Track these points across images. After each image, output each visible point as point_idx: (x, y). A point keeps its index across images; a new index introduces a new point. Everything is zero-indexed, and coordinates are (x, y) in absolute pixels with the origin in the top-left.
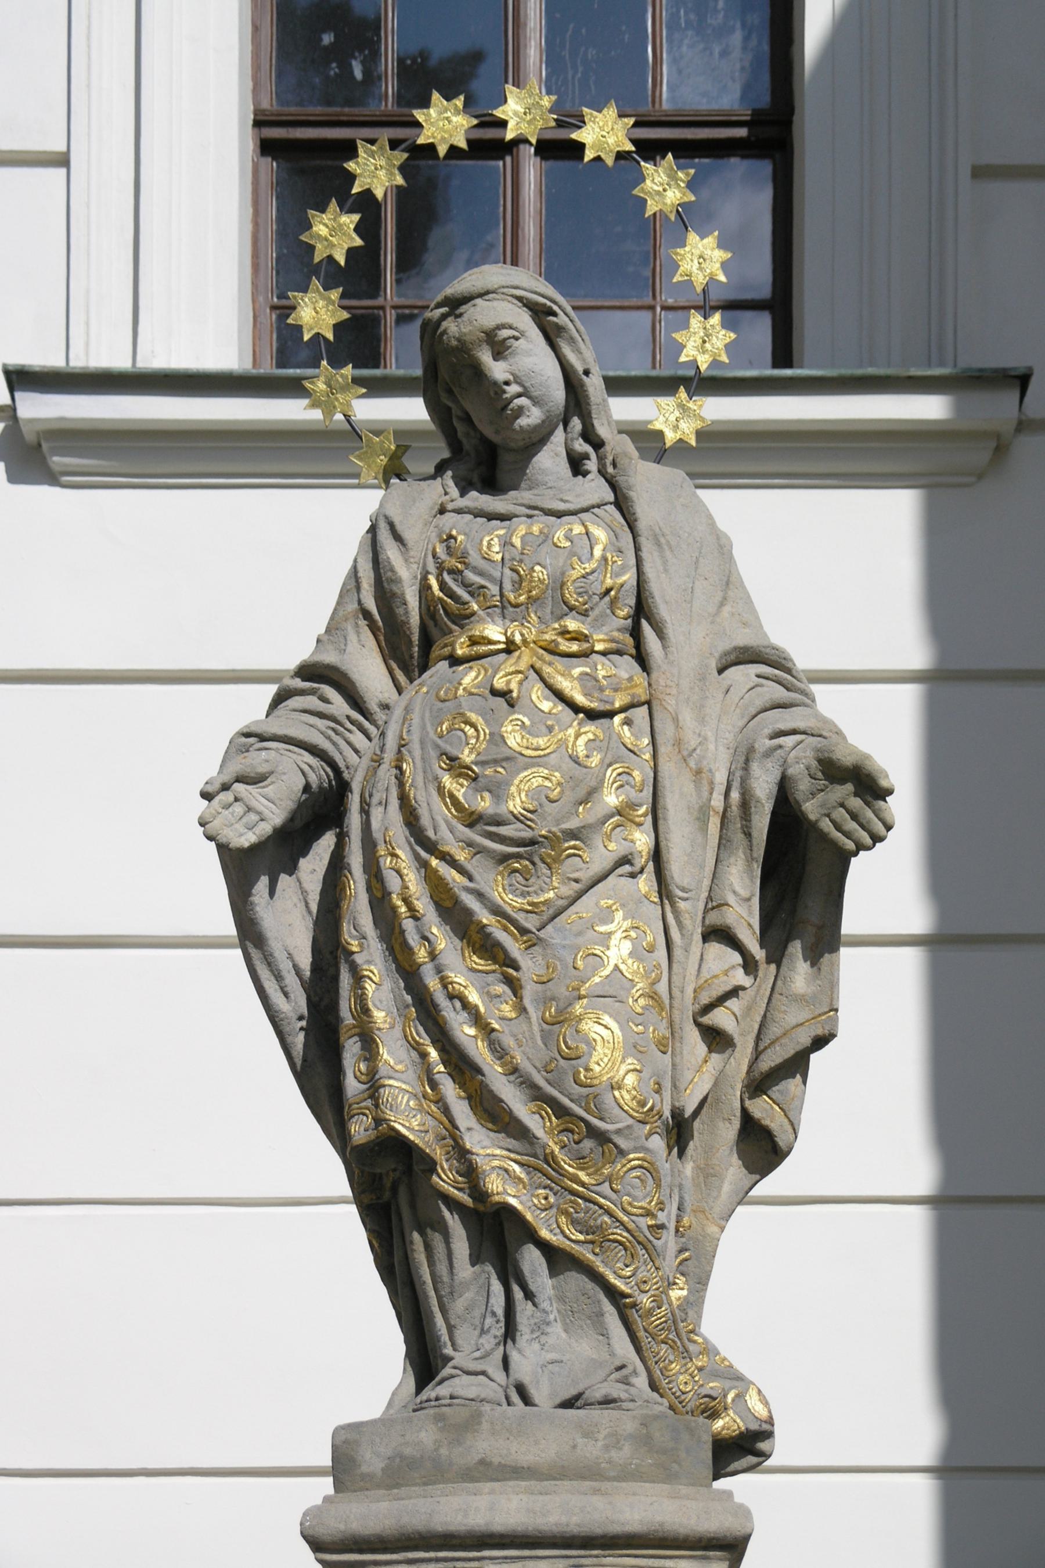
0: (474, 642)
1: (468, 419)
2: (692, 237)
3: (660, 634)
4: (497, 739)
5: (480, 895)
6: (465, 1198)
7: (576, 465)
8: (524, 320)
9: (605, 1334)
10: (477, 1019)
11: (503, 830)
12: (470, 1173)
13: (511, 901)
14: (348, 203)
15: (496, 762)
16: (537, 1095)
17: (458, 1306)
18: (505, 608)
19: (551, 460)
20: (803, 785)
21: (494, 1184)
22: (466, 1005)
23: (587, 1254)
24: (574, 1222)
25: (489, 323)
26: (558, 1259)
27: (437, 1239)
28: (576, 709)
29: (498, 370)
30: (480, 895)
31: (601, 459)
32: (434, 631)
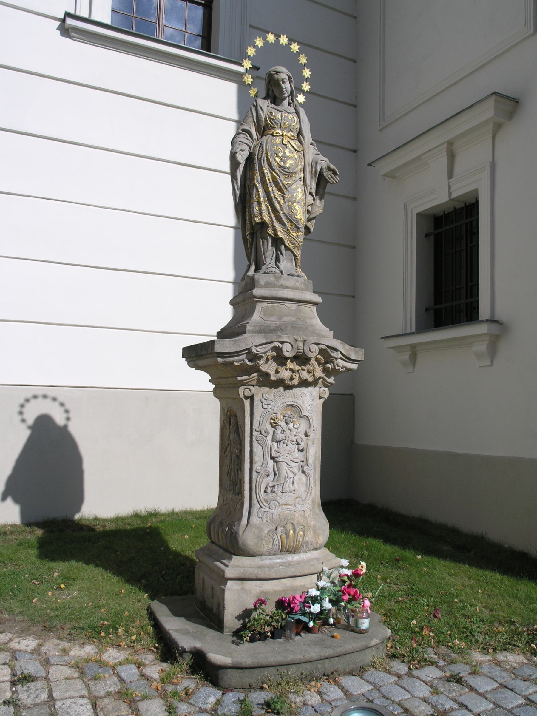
0: (277, 133)
1: (273, 91)
2: (306, 69)
3: (304, 138)
4: (285, 153)
5: (281, 180)
7: (289, 104)
8: (287, 78)
9: (292, 263)
10: (279, 203)
11: (285, 170)
12: (275, 230)
13: (284, 182)
14: (254, 47)
15: (285, 157)
16: (287, 218)
17: (267, 254)
18: (281, 128)
19: (286, 102)
20: (325, 170)
21: (279, 233)
22: (277, 200)
24: (291, 242)
25: (283, 78)
28: (296, 150)
29: (283, 86)
30: (281, 180)
31: (293, 104)
32: (266, 128)
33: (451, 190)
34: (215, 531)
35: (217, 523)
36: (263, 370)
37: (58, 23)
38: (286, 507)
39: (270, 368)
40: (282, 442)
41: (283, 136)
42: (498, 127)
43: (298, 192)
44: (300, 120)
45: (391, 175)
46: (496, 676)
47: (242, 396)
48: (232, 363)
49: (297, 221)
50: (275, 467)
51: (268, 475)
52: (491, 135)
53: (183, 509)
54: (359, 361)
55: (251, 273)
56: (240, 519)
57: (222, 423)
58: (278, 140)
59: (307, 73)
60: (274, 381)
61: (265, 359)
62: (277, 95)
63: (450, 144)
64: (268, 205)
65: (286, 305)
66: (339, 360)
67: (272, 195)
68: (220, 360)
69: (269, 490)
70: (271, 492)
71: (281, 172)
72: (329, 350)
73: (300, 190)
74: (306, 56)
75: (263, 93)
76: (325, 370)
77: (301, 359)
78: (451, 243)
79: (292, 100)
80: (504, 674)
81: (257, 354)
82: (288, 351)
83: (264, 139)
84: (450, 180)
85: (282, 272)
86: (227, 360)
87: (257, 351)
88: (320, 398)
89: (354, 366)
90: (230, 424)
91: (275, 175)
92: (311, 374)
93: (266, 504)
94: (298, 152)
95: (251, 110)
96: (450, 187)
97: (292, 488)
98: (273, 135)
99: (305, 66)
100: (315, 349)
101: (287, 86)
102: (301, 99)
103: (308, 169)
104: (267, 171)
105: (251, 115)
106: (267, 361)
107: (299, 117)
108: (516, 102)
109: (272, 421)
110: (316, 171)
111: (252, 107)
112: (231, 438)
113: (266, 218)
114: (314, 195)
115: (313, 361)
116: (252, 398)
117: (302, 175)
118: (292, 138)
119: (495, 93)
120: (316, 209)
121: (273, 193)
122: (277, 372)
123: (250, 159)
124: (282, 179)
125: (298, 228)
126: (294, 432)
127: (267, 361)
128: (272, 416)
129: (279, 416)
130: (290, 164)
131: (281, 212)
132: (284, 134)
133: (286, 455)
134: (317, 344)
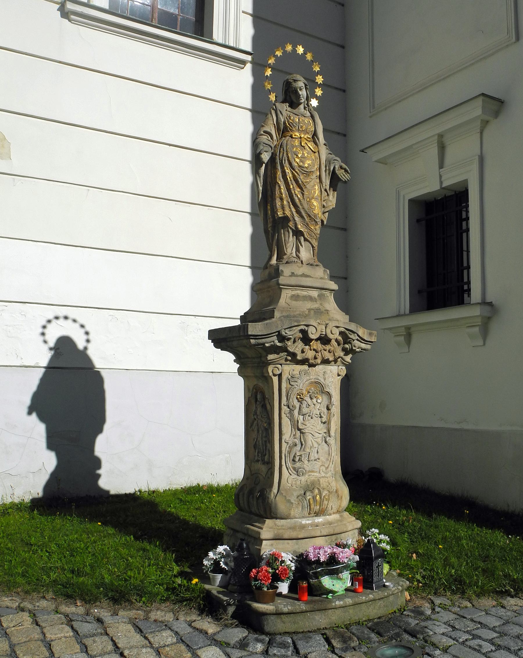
0: (295, 135)
1: (290, 96)
4: (303, 154)
6: (294, 228)
7: (305, 108)
12: (296, 225)
17: (288, 245)
19: (302, 106)
23: (310, 239)
26: (305, 240)
27: (287, 233)
29: (300, 93)
30: (300, 179)
33: (443, 179)
34: (245, 499)
35: (246, 492)
36: (290, 350)
37: (58, 6)
38: (313, 474)
39: (297, 347)
40: (307, 415)
41: (301, 138)
42: (485, 123)
43: (314, 189)
44: (315, 123)
45: (383, 161)
46: (502, 615)
47: (271, 374)
48: (263, 344)
49: (315, 215)
50: (302, 438)
51: (296, 445)
52: (479, 131)
53: (117, 493)
54: (372, 342)
55: (274, 261)
56: (271, 486)
57: (247, 398)
58: (297, 143)
59: (320, 79)
60: (300, 360)
61: (292, 340)
62: (294, 100)
63: (441, 136)
64: (289, 200)
65: (308, 291)
66: (356, 341)
67: (293, 192)
68: (253, 341)
69: (297, 459)
70: (299, 460)
71: (300, 172)
72: (347, 332)
73: (317, 187)
74: (319, 64)
75: (281, 98)
76: (344, 349)
77: (325, 340)
78: (441, 226)
79: (307, 104)
80: (509, 613)
81: (287, 336)
82: (313, 334)
83: (285, 140)
84: (441, 170)
85: (302, 262)
86: (261, 341)
87: (286, 333)
88: (339, 375)
89: (368, 347)
90: (256, 400)
91: (295, 174)
92: (332, 354)
93: (294, 472)
94: (315, 152)
95: (271, 113)
96: (441, 177)
97: (317, 457)
98: (292, 137)
99: (318, 73)
100: (337, 331)
101: (303, 93)
102: (314, 103)
103: (323, 168)
104: (288, 171)
105: (271, 118)
106: (294, 342)
107: (314, 121)
108: (501, 102)
109: (298, 397)
110: (329, 170)
111: (272, 111)
112: (258, 413)
113: (288, 213)
114: (328, 190)
115: (333, 342)
116: (280, 376)
117: (318, 174)
118: (308, 140)
119: (483, 94)
120: (330, 204)
121: (294, 190)
122: (303, 352)
123: (273, 159)
124: (301, 178)
125: (316, 222)
126: (318, 406)
127: (294, 342)
128: (298, 392)
129: (304, 392)
130: (309, 164)
131: (300, 207)
132: (302, 136)
133: (311, 427)
134: (337, 327)
